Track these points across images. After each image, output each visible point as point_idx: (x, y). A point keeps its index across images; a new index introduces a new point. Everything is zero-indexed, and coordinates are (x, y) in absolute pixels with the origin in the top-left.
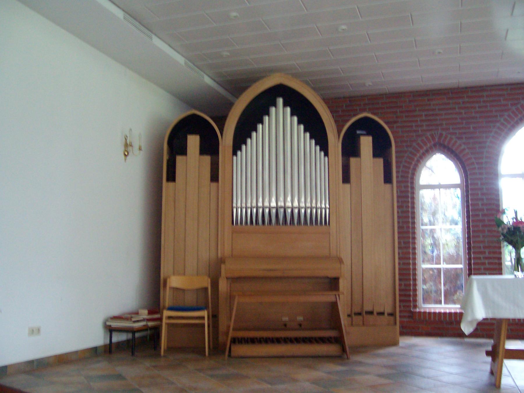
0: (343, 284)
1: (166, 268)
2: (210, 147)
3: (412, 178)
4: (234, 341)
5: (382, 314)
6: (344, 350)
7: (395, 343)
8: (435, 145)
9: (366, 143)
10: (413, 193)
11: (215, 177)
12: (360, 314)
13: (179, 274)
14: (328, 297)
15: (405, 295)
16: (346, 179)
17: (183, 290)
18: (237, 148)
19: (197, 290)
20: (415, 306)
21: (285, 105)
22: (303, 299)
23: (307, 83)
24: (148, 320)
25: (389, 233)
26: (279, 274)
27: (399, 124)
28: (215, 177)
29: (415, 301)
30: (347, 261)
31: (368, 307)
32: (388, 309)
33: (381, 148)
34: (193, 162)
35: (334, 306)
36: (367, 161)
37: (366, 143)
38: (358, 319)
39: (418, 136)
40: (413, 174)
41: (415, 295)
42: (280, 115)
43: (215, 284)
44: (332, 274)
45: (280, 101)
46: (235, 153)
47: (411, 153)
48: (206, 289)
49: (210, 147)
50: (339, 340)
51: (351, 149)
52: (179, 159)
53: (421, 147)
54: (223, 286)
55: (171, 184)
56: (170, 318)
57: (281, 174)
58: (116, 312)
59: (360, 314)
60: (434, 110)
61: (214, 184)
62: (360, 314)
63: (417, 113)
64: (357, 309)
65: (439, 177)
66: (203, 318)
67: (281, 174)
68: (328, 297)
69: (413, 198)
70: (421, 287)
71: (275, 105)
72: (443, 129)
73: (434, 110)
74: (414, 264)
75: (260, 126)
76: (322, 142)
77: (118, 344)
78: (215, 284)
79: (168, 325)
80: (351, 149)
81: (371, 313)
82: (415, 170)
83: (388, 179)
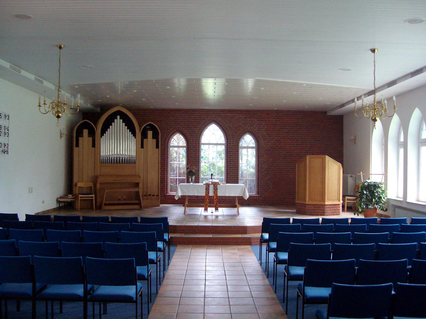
0: (140, 185)
1: (75, 180)
2: (92, 133)
3: (168, 143)
4: (105, 204)
5: (154, 195)
6: (141, 207)
7: (159, 206)
8: (177, 131)
9: (150, 133)
10: (167, 149)
11: (94, 145)
12: (146, 195)
13: (80, 182)
14: (136, 190)
15: (163, 189)
16: (142, 147)
17: (82, 187)
18: (102, 135)
19: (88, 187)
20: (167, 193)
21: (120, 119)
22: (123, 190)
23: (127, 109)
24: (72, 198)
25: (157, 166)
26: (118, 181)
27: (163, 122)
28: (94, 145)
29: (167, 191)
30: (142, 177)
31: (149, 193)
32: (156, 194)
33: (155, 136)
34: (85, 140)
35: (138, 192)
36: (150, 141)
37: (150, 133)
38: (144, 197)
39: (171, 127)
40: (168, 142)
41: (167, 189)
42: (119, 122)
43: (95, 186)
44: (137, 181)
45: (118, 117)
46: (101, 137)
47: (167, 134)
48: (91, 187)
49: (92, 133)
50: (139, 204)
51: (144, 135)
52: (80, 139)
53: (171, 132)
54: (98, 186)
55: (77, 148)
56: (81, 197)
57: (118, 145)
58: (59, 196)
59: (146, 195)
60: (177, 117)
61: (93, 148)
62: (146, 195)
63: (170, 118)
64: (145, 194)
65: (178, 141)
66: (92, 197)
67: (118, 145)
68: (136, 190)
69: (167, 151)
70: (169, 184)
71: (116, 118)
72: (180, 125)
73: (177, 117)
74: (167, 177)
75: (111, 127)
76: (134, 133)
77: (62, 206)
78: (95, 186)
79: (80, 200)
80: (144, 135)
81: (150, 195)
82: (169, 138)
83: (157, 147)
